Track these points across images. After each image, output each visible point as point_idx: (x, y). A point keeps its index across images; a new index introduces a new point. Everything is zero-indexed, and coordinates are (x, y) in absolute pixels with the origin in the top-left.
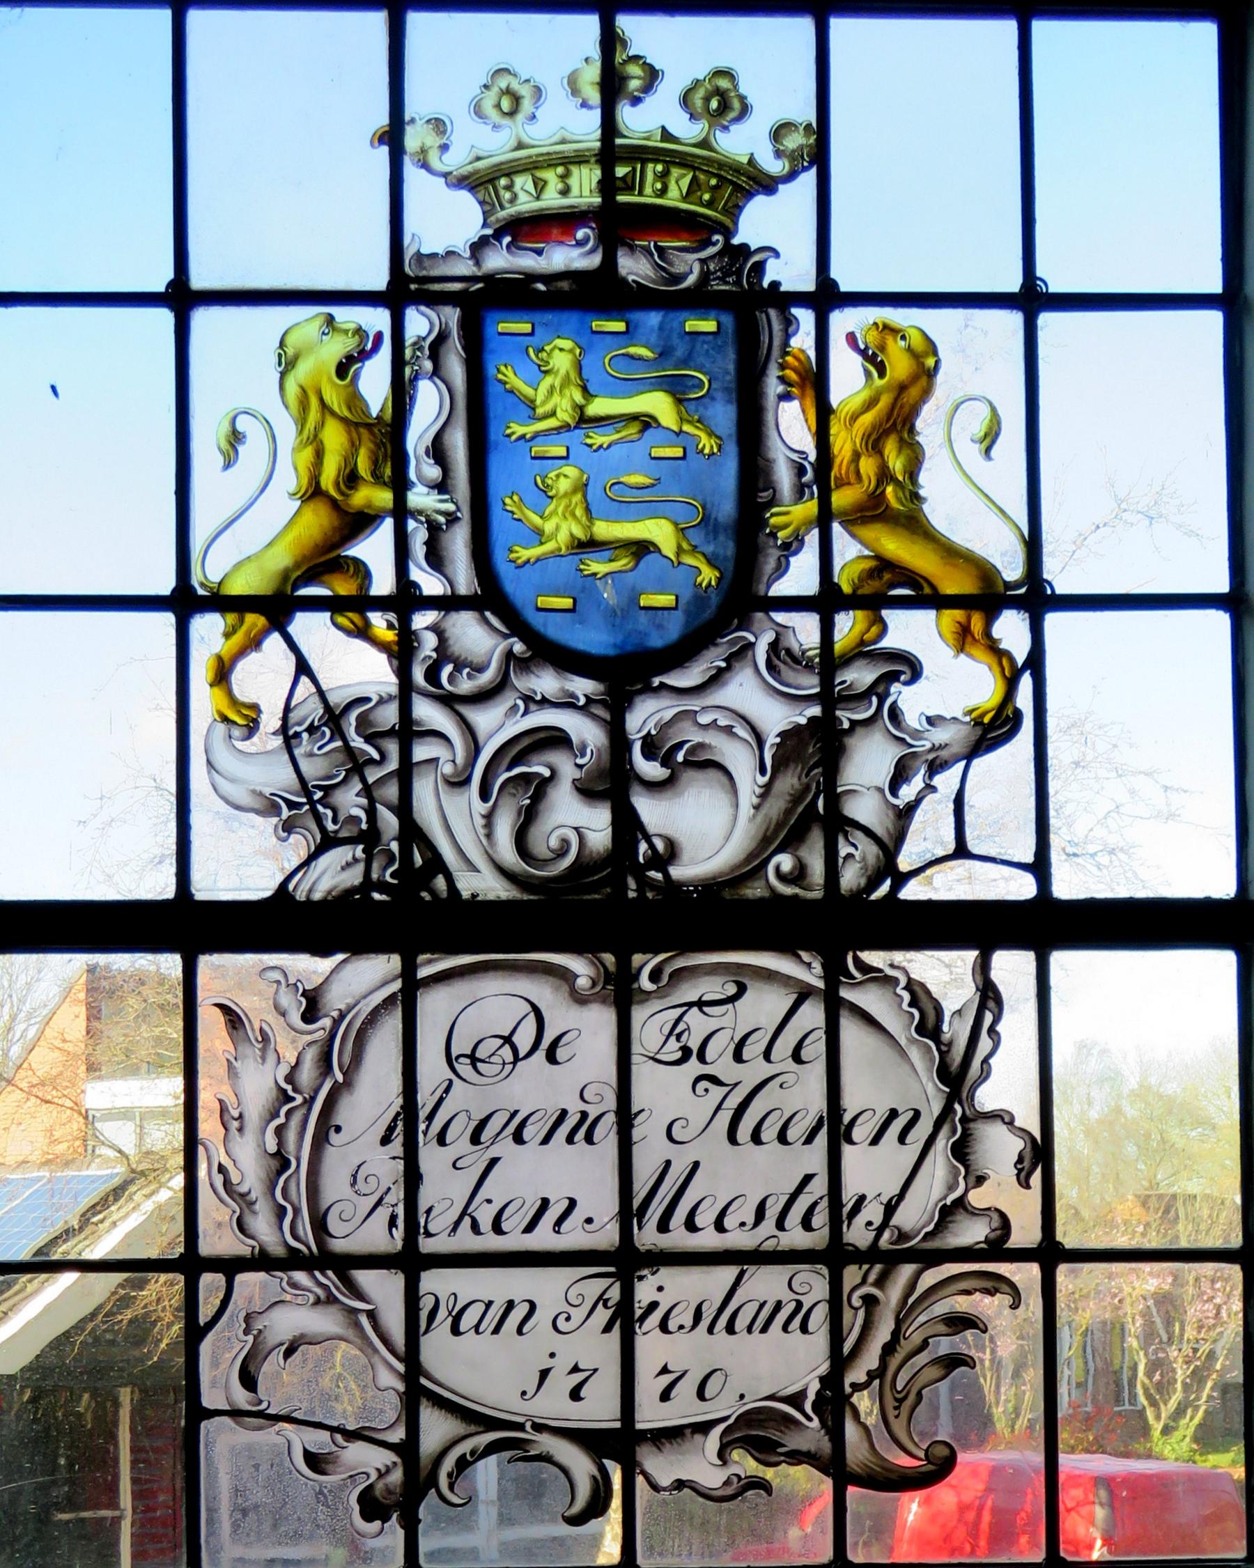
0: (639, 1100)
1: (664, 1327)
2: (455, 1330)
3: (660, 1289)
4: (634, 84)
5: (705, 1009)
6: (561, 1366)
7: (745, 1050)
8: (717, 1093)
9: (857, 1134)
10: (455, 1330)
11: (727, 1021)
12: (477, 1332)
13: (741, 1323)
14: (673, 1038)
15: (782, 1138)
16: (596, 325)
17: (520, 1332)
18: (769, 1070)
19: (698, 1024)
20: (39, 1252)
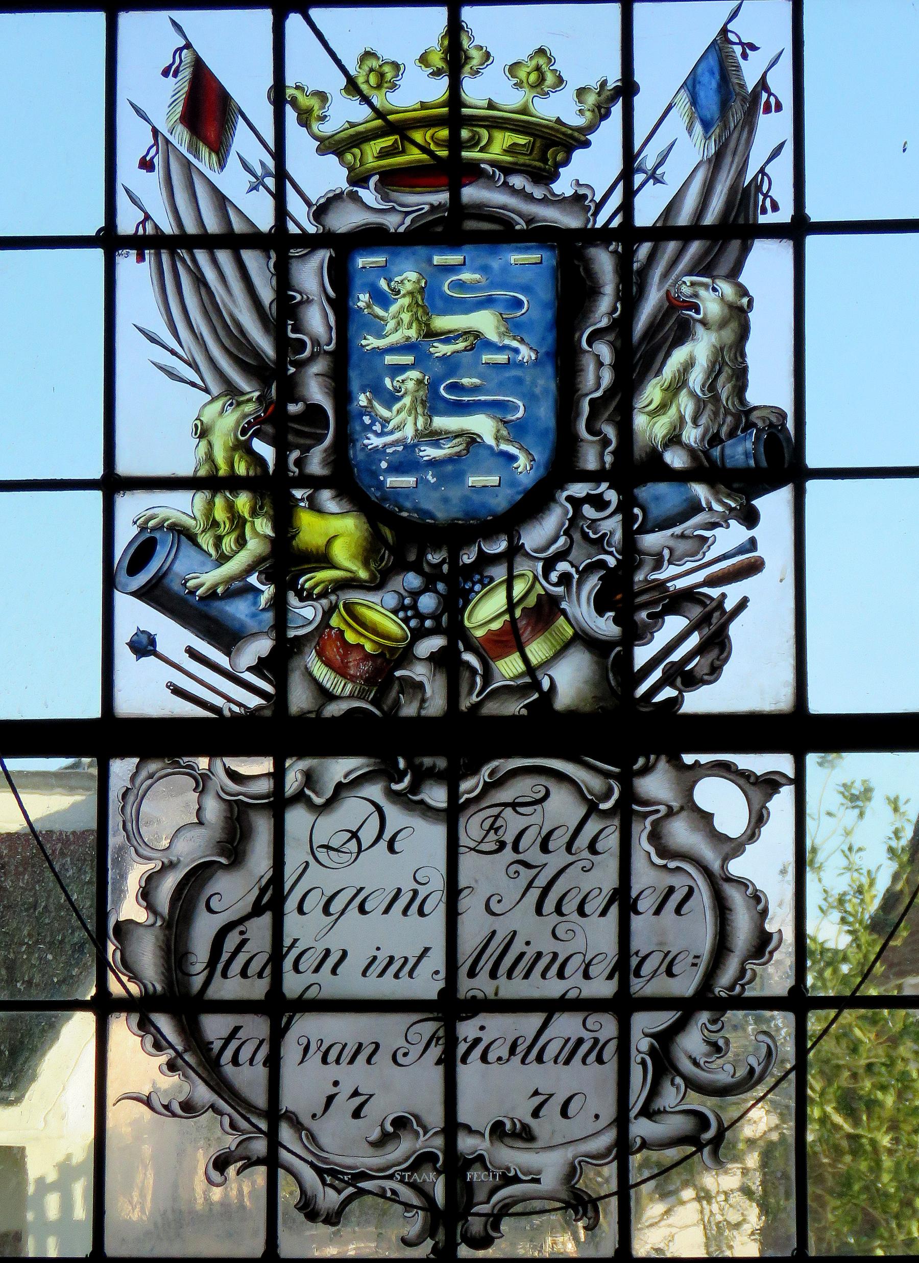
0: (463, 881)
1: (484, 1058)
2: (324, 1061)
3: (482, 1028)
4: (475, 62)
5: (518, 809)
6: (346, 1089)
8: (526, 874)
9: (641, 906)
11: (536, 819)
13: (549, 1054)
14: (492, 832)
15: (581, 911)
16: (437, 259)
17: (369, 1061)
18: (571, 858)
19: (513, 823)
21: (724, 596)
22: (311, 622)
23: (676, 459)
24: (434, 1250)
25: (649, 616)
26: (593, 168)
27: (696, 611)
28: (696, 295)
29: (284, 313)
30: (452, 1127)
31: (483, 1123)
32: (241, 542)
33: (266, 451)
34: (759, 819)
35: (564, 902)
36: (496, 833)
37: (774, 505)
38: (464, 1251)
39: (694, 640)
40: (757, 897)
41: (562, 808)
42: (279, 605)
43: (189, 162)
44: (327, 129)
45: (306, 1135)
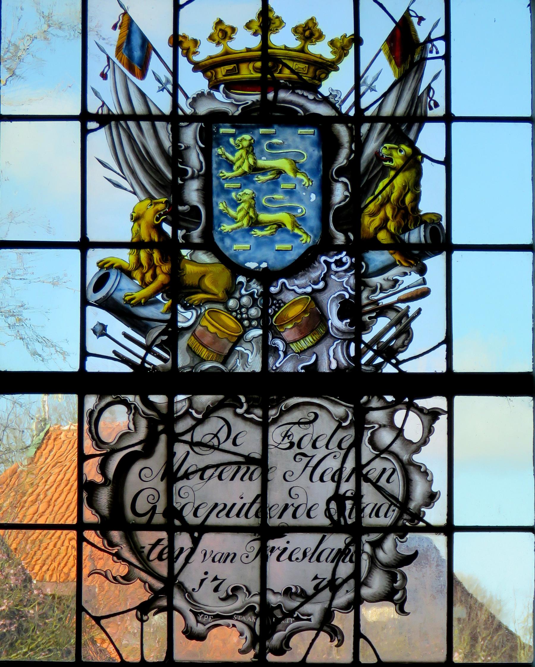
1: (290, 558)
2: (213, 561)
3: (288, 542)
5: (301, 426)
7: (223, 475)
8: (305, 460)
10: (213, 561)
11: (310, 430)
12: (219, 562)
18: (329, 451)
20: (459, 583)
21: (408, 307)
22: (189, 320)
23: (382, 236)
24: (255, 656)
25: (370, 318)
26: (338, 83)
27: (393, 315)
28: (391, 154)
29: (176, 156)
30: (264, 590)
31: (280, 588)
32: (154, 276)
33: (167, 229)
34: (429, 431)
35: (325, 474)
36: (288, 439)
37: (435, 264)
38: (271, 658)
39: (393, 331)
40: (426, 473)
41: (324, 426)
42: (173, 310)
43: (125, 75)
44: (196, 58)
45: (188, 595)
